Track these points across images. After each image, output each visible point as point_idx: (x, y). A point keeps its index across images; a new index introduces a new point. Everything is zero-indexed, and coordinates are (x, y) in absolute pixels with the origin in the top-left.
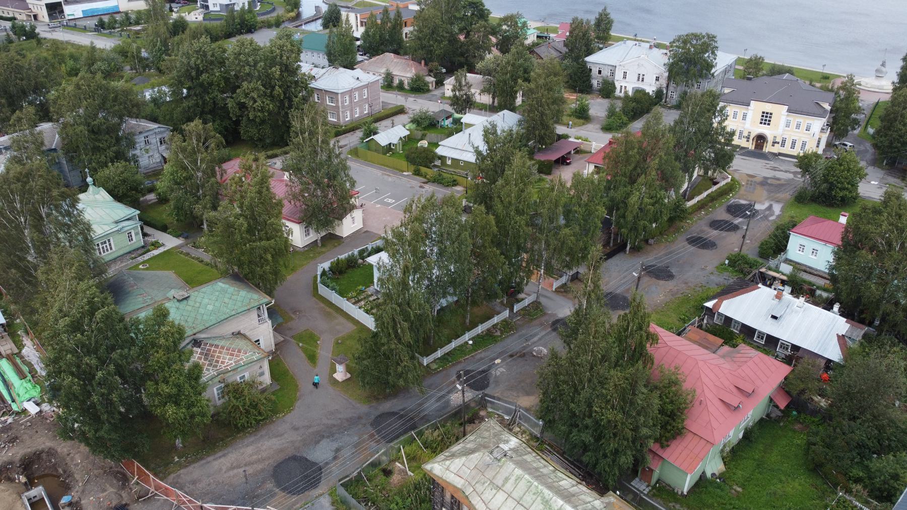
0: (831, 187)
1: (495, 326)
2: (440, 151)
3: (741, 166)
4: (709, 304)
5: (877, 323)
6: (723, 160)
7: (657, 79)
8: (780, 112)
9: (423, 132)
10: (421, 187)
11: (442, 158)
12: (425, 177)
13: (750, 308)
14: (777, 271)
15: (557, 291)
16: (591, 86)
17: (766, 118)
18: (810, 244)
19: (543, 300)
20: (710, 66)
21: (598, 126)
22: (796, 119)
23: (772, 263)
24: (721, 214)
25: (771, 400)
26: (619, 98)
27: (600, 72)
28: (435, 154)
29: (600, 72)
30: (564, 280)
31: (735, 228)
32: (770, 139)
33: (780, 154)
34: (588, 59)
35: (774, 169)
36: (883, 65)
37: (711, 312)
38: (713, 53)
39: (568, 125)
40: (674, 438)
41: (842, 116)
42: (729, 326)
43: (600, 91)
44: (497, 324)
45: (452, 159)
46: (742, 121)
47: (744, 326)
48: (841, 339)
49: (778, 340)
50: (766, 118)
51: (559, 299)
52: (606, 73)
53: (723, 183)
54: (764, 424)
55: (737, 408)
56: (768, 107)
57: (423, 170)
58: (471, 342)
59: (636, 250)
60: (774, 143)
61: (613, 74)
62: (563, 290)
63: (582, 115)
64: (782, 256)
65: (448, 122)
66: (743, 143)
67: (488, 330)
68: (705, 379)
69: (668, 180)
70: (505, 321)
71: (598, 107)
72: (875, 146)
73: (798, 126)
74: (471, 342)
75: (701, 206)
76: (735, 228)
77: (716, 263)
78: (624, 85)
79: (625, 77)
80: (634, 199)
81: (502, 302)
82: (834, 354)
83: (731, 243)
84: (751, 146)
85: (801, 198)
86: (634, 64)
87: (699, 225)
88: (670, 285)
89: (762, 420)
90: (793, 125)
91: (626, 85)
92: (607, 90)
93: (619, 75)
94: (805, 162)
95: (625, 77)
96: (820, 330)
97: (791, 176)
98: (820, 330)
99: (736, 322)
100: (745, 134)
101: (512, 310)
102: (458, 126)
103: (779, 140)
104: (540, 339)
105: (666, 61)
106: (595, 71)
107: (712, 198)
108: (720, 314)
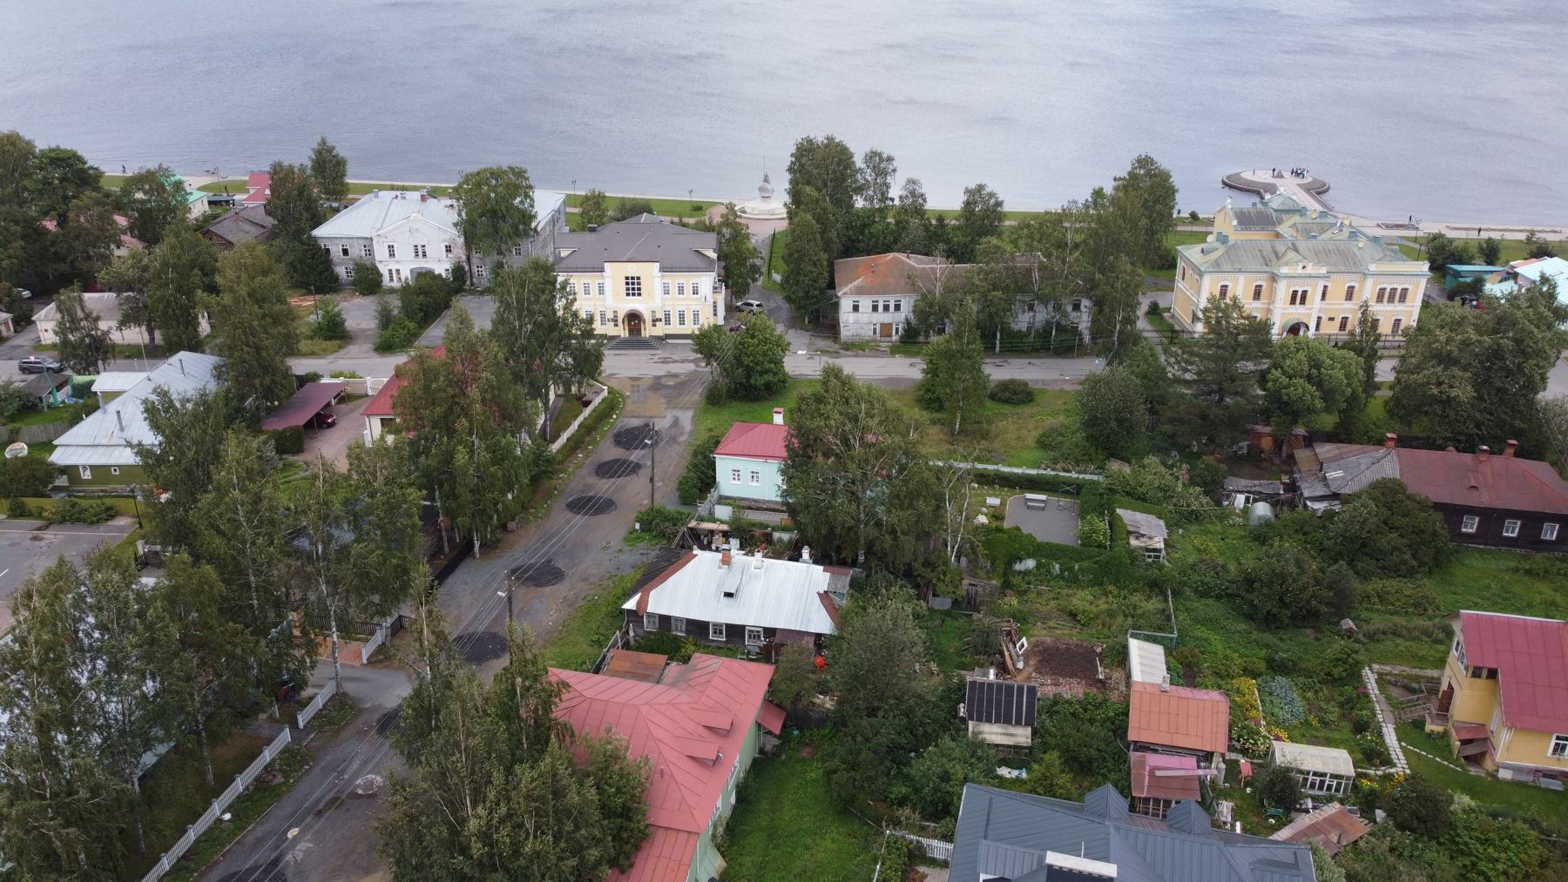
0: (749, 372)
1: (268, 768)
2: (59, 457)
3: (618, 366)
4: (630, 604)
5: (861, 558)
6: (588, 364)
7: (448, 249)
8: (650, 273)
9: (11, 426)
10: (35, 538)
11: (70, 471)
12: (40, 516)
13: (692, 591)
14: (714, 520)
15: (372, 662)
16: (336, 278)
17: (633, 286)
18: (746, 465)
19: (350, 688)
20: (527, 217)
21: (368, 346)
22: (675, 279)
23: (702, 509)
24: (609, 451)
25: (759, 726)
26: (392, 291)
27: (345, 252)
28: (52, 464)
29: (345, 252)
30: (379, 637)
31: (635, 468)
32: (648, 317)
33: (668, 336)
34: (318, 232)
35: (665, 361)
36: (766, 180)
37: (635, 616)
38: (527, 196)
39: (312, 354)
40: (637, 848)
41: (735, 270)
42: (669, 630)
43: (353, 283)
44: (273, 760)
45: (92, 467)
46: (597, 296)
47: (690, 622)
48: (825, 597)
49: (743, 627)
50: (633, 286)
51: (379, 676)
52: (357, 251)
53: (597, 401)
54: (761, 765)
55: (717, 760)
56: (632, 269)
57: (32, 503)
58: (227, 816)
59: (489, 547)
60: (655, 321)
61: (370, 252)
62: (382, 657)
63: (335, 333)
64: (713, 495)
65: (62, 396)
66: (610, 330)
67: (258, 780)
68: (658, 733)
69: (513, 418)
70: (286, 750)
71: (359, 313)
72: (788, 299)
73: (681, 290)
74: (227, 816)
75: (575, 444)
76: (635, 468)
77: (623, 533)
78: (394, 267)
79: (392, 254)
80: (461, 456)
81: (271, 718)
82: (822, 623)
83: (634, 493)
84: (622, 332)
85: (715, 399)
86: (400, 231)
87: (579, 478)
88: (562, 590)
89: (755, 762)
90: (674, 290)
91: (398, 268)
92: (368, 280)
93: (380, 253)
94: (705, 343)
95: (392, 254)
96: (789, 594)
97: (691, 367)
98: (789, 594)
99: (678, 619)
100: (610, 315)
101: (294, 724)
102: (88, 403)
103: (660, 315)
104: (365, 763)
105: (456, 218)
106: (336, 252)
107: (588, 429)
108: (651, 615)
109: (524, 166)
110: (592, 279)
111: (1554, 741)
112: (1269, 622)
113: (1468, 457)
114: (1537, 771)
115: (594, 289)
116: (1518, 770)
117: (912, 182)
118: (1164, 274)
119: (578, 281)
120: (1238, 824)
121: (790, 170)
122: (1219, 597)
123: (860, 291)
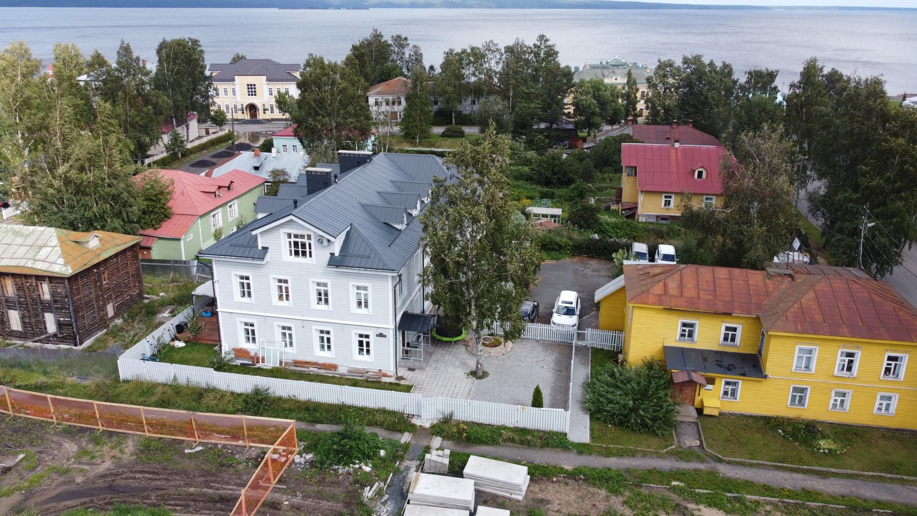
17: (252, 90)
33: (273, 120)
50: (252, 90)
56: (251, 80)
66: (239, 116)
84: (247, 116)
100: (239, 107)
109: (197, 38)
110: (228, 86)
111: (664, 199)
112: (547, 183)
113: (667, 127)
114: (658, 217)
115: (230, 92)
116: (649, 216)
117: (415, 46)
118: (617, 175)
119: (221, 87)
120: (674, 483)
121: (355, 48)
122: (526, 180)
123: (379, 93)
